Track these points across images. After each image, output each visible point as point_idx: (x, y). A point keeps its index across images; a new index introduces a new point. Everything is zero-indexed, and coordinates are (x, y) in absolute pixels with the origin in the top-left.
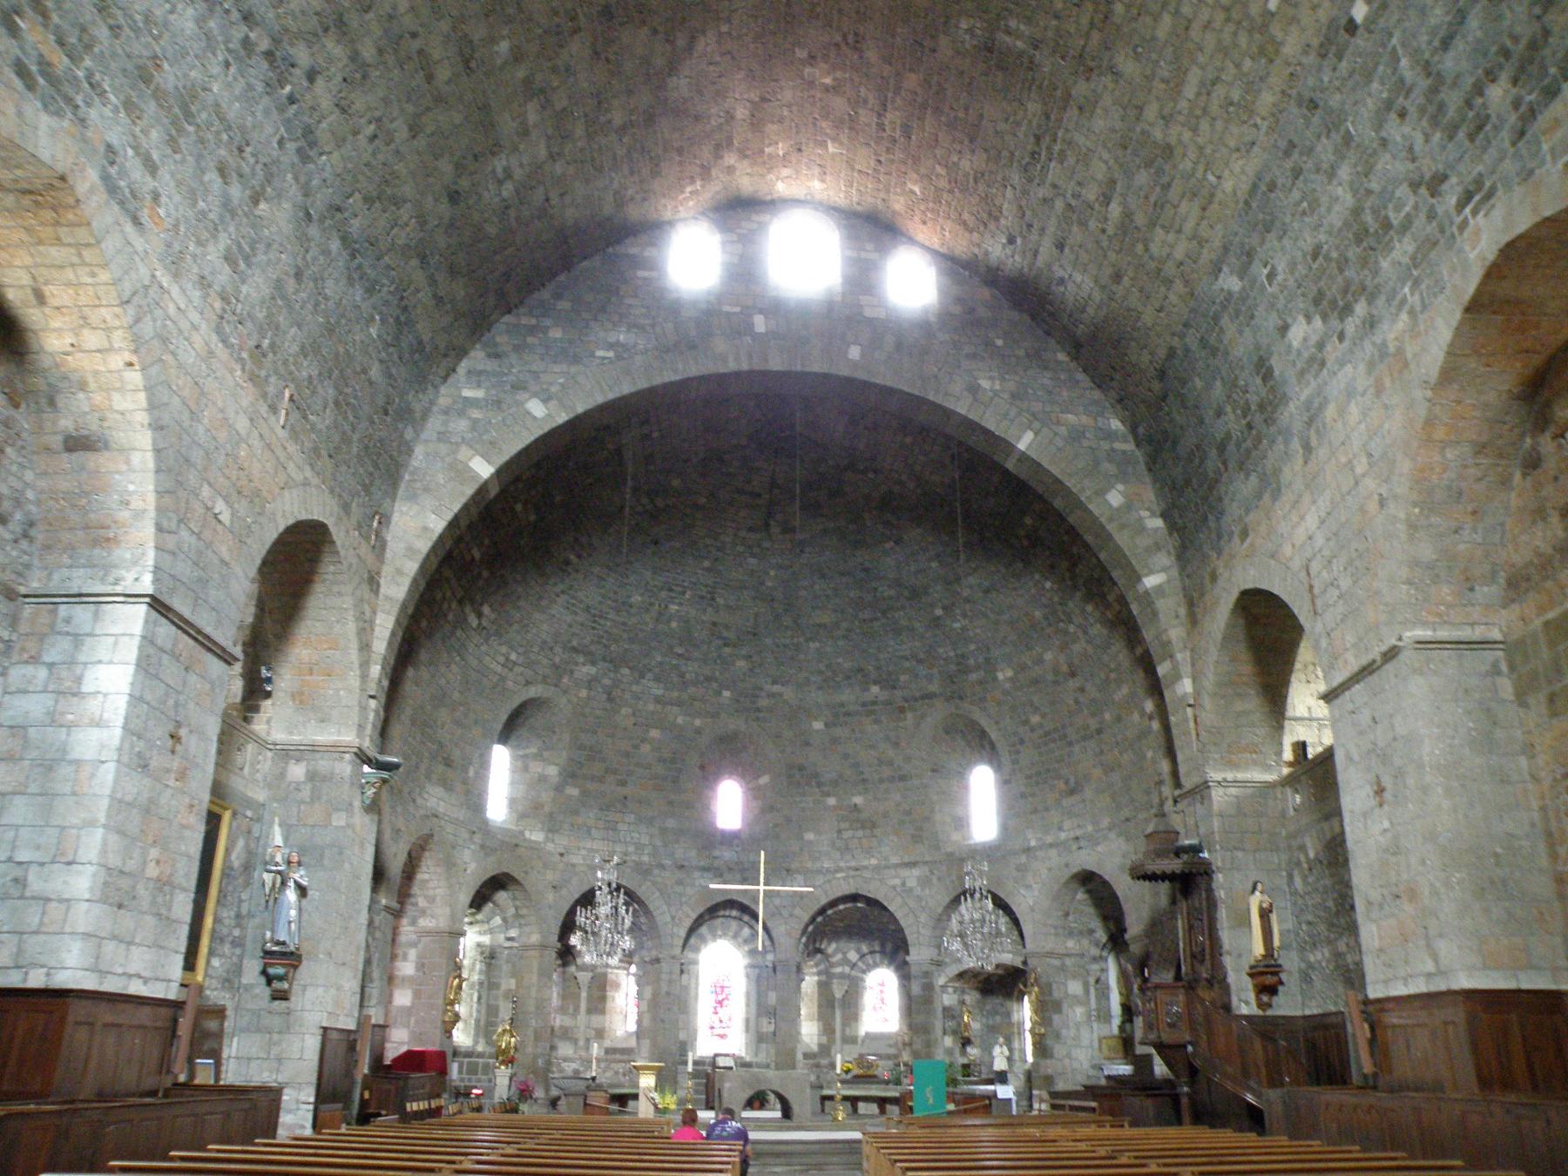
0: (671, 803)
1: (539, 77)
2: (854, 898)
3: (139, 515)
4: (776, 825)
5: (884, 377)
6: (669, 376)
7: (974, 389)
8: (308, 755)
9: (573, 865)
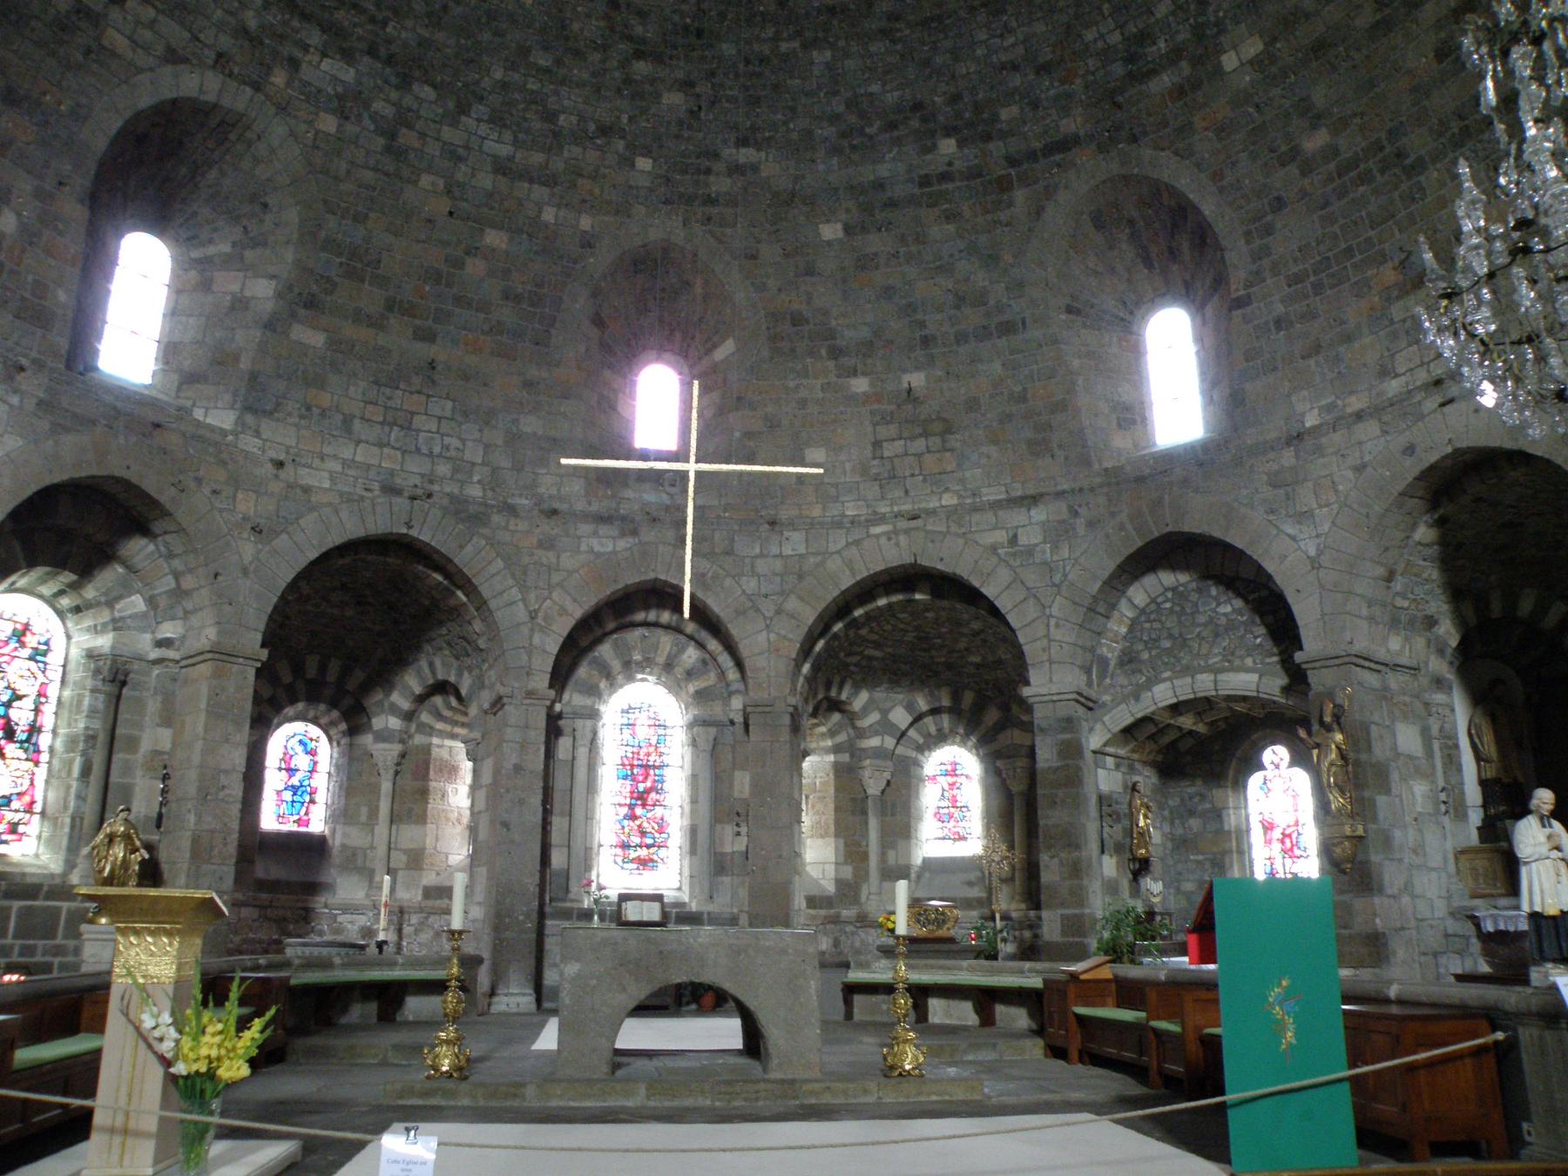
0: (529, 385)
2: (906, 578)
4: (748, 435)
9: (307, 490)
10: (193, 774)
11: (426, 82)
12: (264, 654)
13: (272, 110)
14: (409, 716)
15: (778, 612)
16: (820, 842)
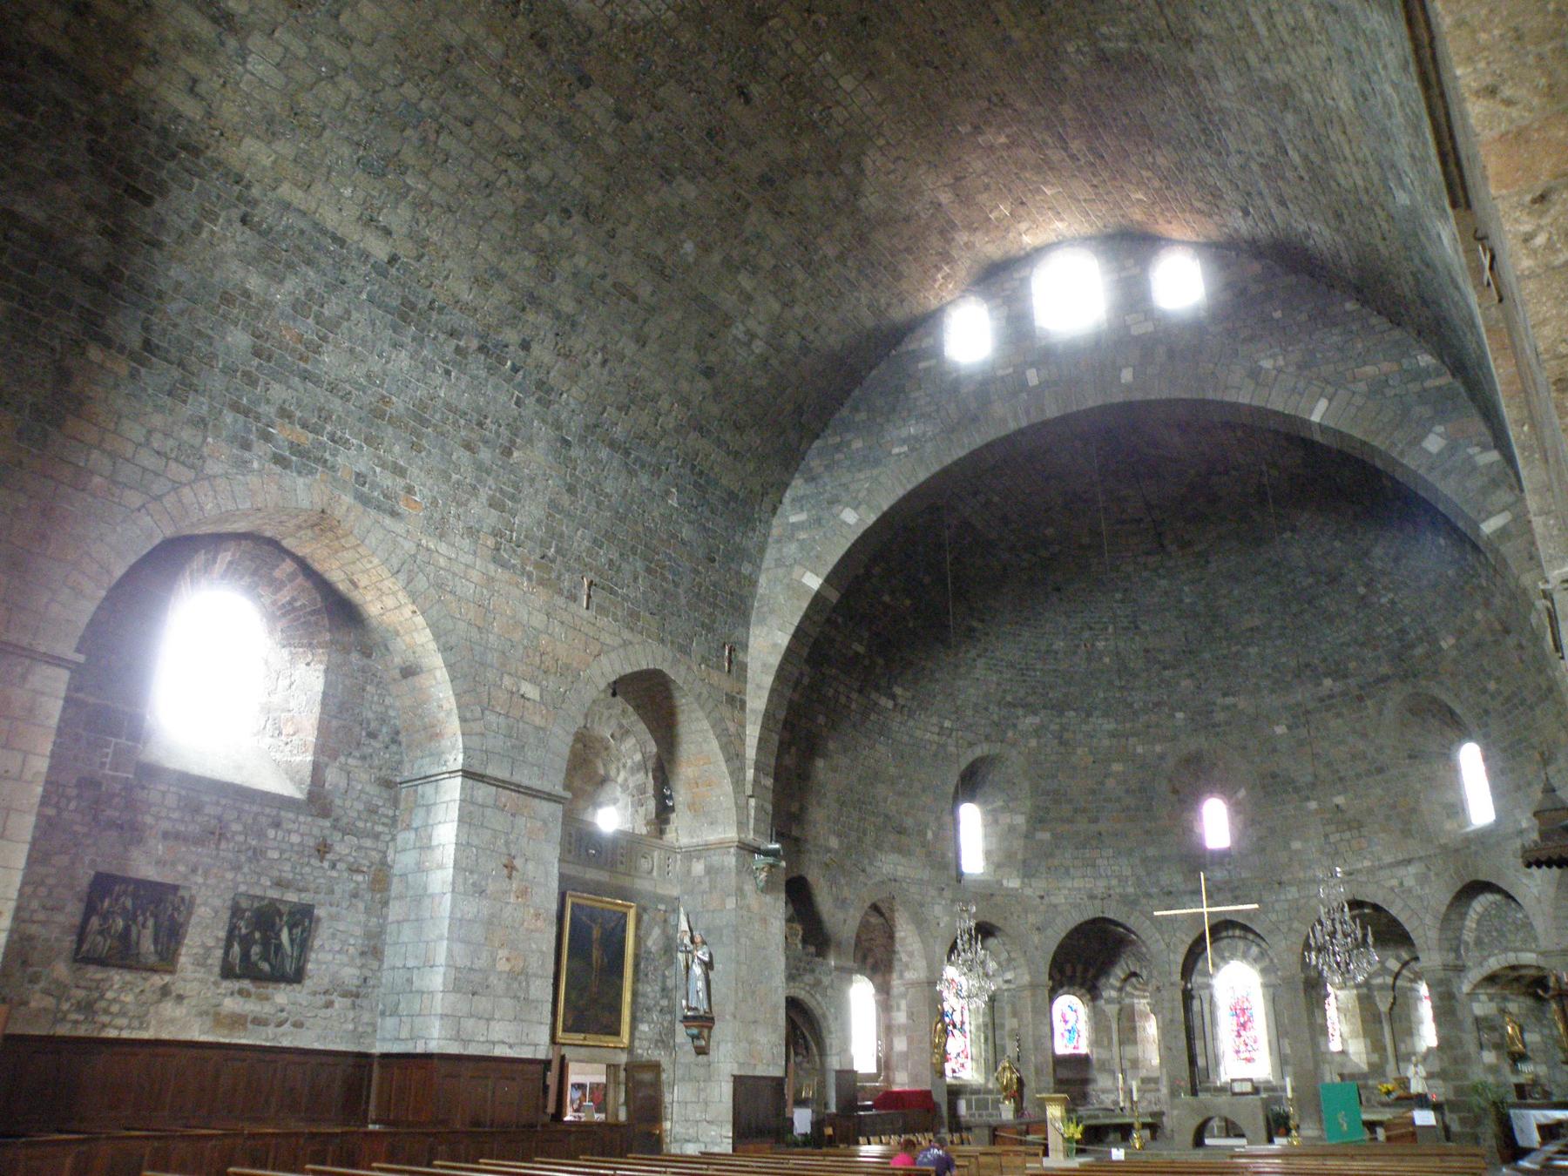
0: (1147, 832)
1: (735, 253)
3: (449, 713)
4: (1261, 838)
5: (1160, 391)
6: (960, 453)
7: (1255, 374)
8: (704, 853)
9: (1055, 906)
10: (1030, 1039)
12: (1050, 983)
14: (1120, 989)
15: (1290, 929)
16: (1355, 1041)
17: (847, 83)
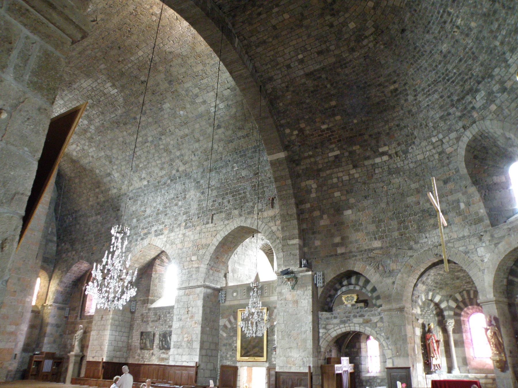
11: (494, 69)
13: (482, 122)
17: (140, 53)
